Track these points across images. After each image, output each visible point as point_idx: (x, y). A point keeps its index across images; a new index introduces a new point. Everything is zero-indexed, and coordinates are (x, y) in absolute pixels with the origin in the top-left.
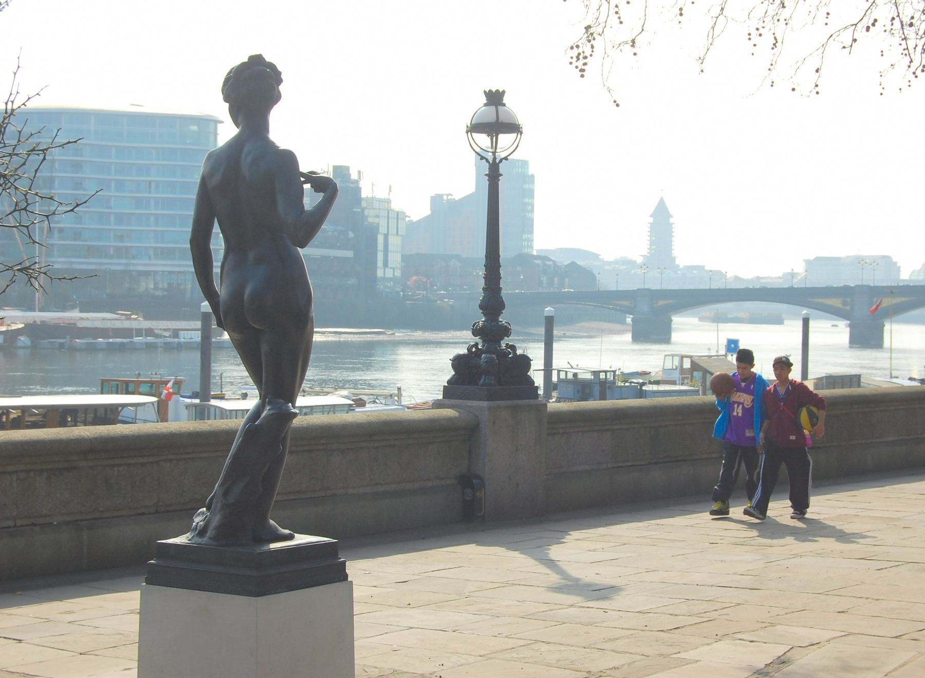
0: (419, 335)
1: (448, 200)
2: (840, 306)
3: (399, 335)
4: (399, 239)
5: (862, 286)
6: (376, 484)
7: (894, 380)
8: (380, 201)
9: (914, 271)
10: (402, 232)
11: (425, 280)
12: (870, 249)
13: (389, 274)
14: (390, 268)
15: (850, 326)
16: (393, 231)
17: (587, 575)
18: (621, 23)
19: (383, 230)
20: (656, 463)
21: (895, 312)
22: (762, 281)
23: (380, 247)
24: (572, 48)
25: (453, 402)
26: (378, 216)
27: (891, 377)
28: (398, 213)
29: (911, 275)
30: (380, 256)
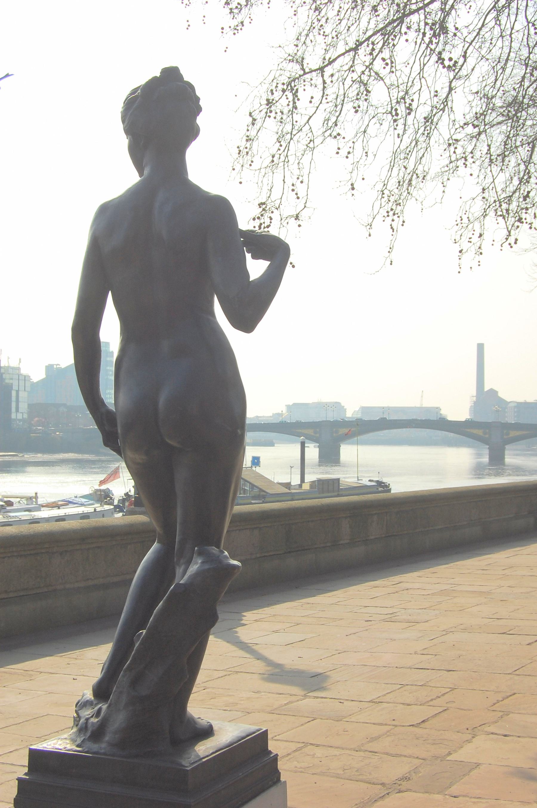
0: (40, 457)
3: (28, 457)
4: (26, 393)
6: (88, 579)
7: (359, 482)
8: (13, 368)
10: (28, 389)
11: (44, 420)
12: (328, 398)
13: (20, 416)
14: (20, 413)
15: (319, 447)
16: (22, 388)
17: (289, 659)
19: (15, 387)
20: (290, 552)
22: (260, 419)
23: (14, 398)
24: (254, 219)
26: (12, 379)
28: (25, 376)
29: (352, 415)
30: (14, 405)
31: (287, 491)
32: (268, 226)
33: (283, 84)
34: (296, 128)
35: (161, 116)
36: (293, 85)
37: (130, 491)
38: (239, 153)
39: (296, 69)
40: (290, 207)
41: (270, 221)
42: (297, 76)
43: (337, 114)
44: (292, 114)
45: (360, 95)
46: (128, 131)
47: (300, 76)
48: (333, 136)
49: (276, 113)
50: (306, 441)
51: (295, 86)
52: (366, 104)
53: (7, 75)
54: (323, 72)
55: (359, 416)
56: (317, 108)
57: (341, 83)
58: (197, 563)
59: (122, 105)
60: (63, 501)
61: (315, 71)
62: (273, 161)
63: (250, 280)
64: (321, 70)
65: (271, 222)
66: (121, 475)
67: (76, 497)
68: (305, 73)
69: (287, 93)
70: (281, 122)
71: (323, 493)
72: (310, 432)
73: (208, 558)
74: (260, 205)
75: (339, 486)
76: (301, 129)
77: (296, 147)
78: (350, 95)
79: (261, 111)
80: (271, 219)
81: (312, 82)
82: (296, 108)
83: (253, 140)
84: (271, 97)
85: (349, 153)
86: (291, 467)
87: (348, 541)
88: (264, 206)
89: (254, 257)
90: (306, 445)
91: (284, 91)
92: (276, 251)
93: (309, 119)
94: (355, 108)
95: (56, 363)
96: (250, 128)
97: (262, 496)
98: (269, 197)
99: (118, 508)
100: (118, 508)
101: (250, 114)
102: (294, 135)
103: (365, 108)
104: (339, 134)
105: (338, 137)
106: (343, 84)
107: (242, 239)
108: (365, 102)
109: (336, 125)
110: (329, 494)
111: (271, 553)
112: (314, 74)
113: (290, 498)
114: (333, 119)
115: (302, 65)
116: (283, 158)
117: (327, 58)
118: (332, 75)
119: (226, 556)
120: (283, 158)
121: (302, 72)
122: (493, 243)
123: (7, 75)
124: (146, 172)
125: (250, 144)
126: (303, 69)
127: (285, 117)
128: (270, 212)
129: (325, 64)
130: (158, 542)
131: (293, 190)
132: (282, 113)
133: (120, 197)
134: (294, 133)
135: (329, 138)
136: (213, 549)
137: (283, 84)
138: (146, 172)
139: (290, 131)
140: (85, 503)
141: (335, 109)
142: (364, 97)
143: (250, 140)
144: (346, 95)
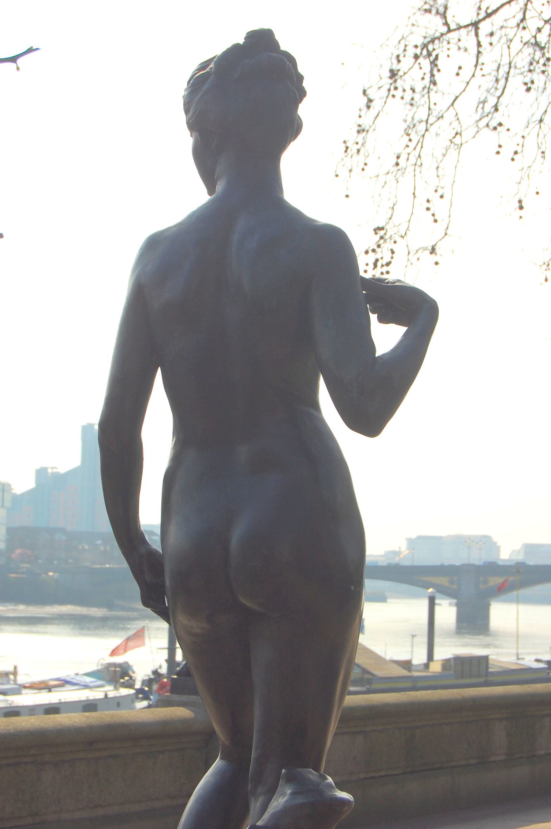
0: (22, 610)
1: (53, 474)
2: (447, 584)
5: (469, 565)
7: (520, 662)
9: (514, 551)
15: (458, 605)
18: (436, 221)
20: (411, 772)
21: (501, 591)
25: (184, 698)
27: (518, 659)
29: (510, 555)
31: (405, 673)
32: (388, 264)
33: (416, 47)
34: (435, 113)
35: (246, 102)
36: (430, 47)
37: (160, 667)
38: (346, 151)
39: (435, 25)
40: (423, 233)
41: (390, 255)
42: (438, 34)
43: (498, 93)
44: (428, 92)
45: (535, 64)
46: (194, 125)
47: (442, 35)
48: (491, 127)
49: (404, 91)
50: (438, 595)
51: (434, 49)
52: (542, 77)
53: (30, 50)
54: (477, 29)
55: (520, 557)
56: (468, 83)
57: (505, 47)
58: (284, 794)
59: (185, 86)
60: (58, 679)
61: (465, 27)
62: (397, 164)
63: (376, 356)
64: (475, 25)
65: (392, 258)
66: (147, 640)
67: (77, 674)
68: (449, 31)
69: (421, 60)
70: (412, 105)
71: (462, 677)
72: (444, 581)
73: (302, 787)
74: (377, 230)
75: (487, 667)
76: (442, 117)
77: (435, 144)
78: (518, 66)
79: (380, 88)
80: (393, 252)
81: (461, 44)
82: (435, 84)
83: (368, 131)
84: (395, 67)
85: (516, 153)
86: (413, 636)
87: (503, 758)
88: (382, 233)
89: (381, 320)
90: (437, 601)
91: (416, 57)
92: (416, 311)
93: (455, 100)
94: (526, 84)
95: (53, 466)
96: (362, 114)
97: (369, 682)
98: (390, 219)
99: (143, 694)
100: (143, 694)
101: (364, 92)
102: (431, 125)
103: (542, 85)
104: (500, 124)
105: (499, 128)
106: (509, 47)
107: (364, 292)
108: (541, 75)
109: (496, 110)
110: (474, 681)
111: (383, 773)
112: (463, 31)
113: (409, 685)
114: (492, 101)
115: (445, 18)
116: (413, 160)
117: (484, 8)
118: (492, 34)
119: (330, 785)
120: (413, 160)
121: (445, 29)
122: (500, 150)
123: (30, 50)
124: (220, 187)
125: (364, 138)
126: (446, 24)
127: (417, 96)
128: (392, 241)
129: (481, 17)
130: (221, 758)
131: (428, 209)
132: (413, 90)
133: (179, 224)
134: (430, 121)
135: (486, 129)
136: (310, 772)
137: (416, 47)
138: (220, 187)
139: (425, 118)
140: (91, 685)
141: (495, 85)
142: (539, 68)
143: (364, 130)
144: (512, 65)
